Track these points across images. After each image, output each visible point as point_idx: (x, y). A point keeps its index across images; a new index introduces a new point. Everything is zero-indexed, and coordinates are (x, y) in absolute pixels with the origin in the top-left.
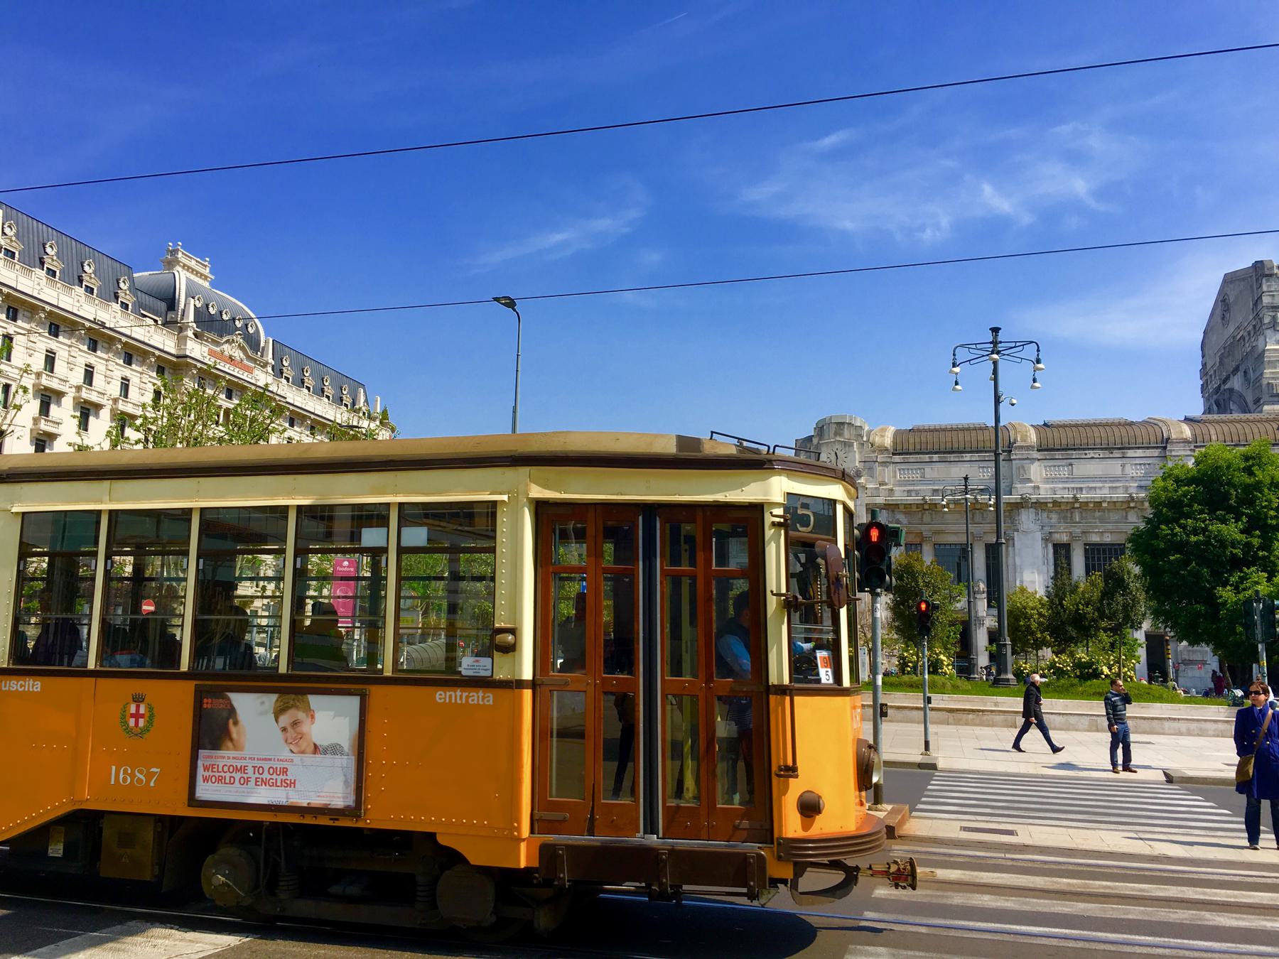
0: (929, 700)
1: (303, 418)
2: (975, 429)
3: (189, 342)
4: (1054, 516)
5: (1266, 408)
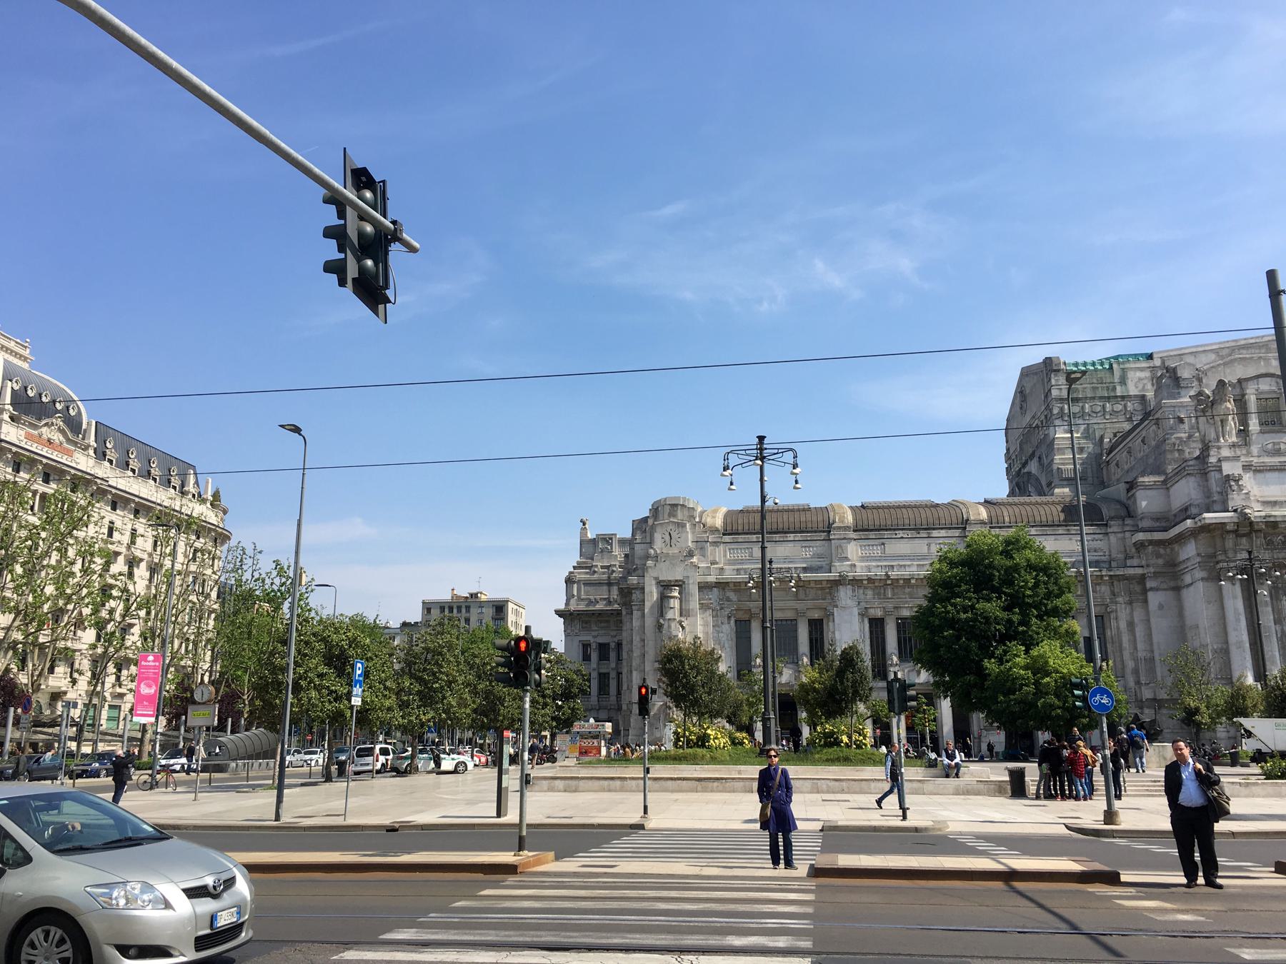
0: (648, 771)
1: (126, 502)
2: (799, 510)
3: (4, 425)
4: (870, 592)
5: (1057, 490)
